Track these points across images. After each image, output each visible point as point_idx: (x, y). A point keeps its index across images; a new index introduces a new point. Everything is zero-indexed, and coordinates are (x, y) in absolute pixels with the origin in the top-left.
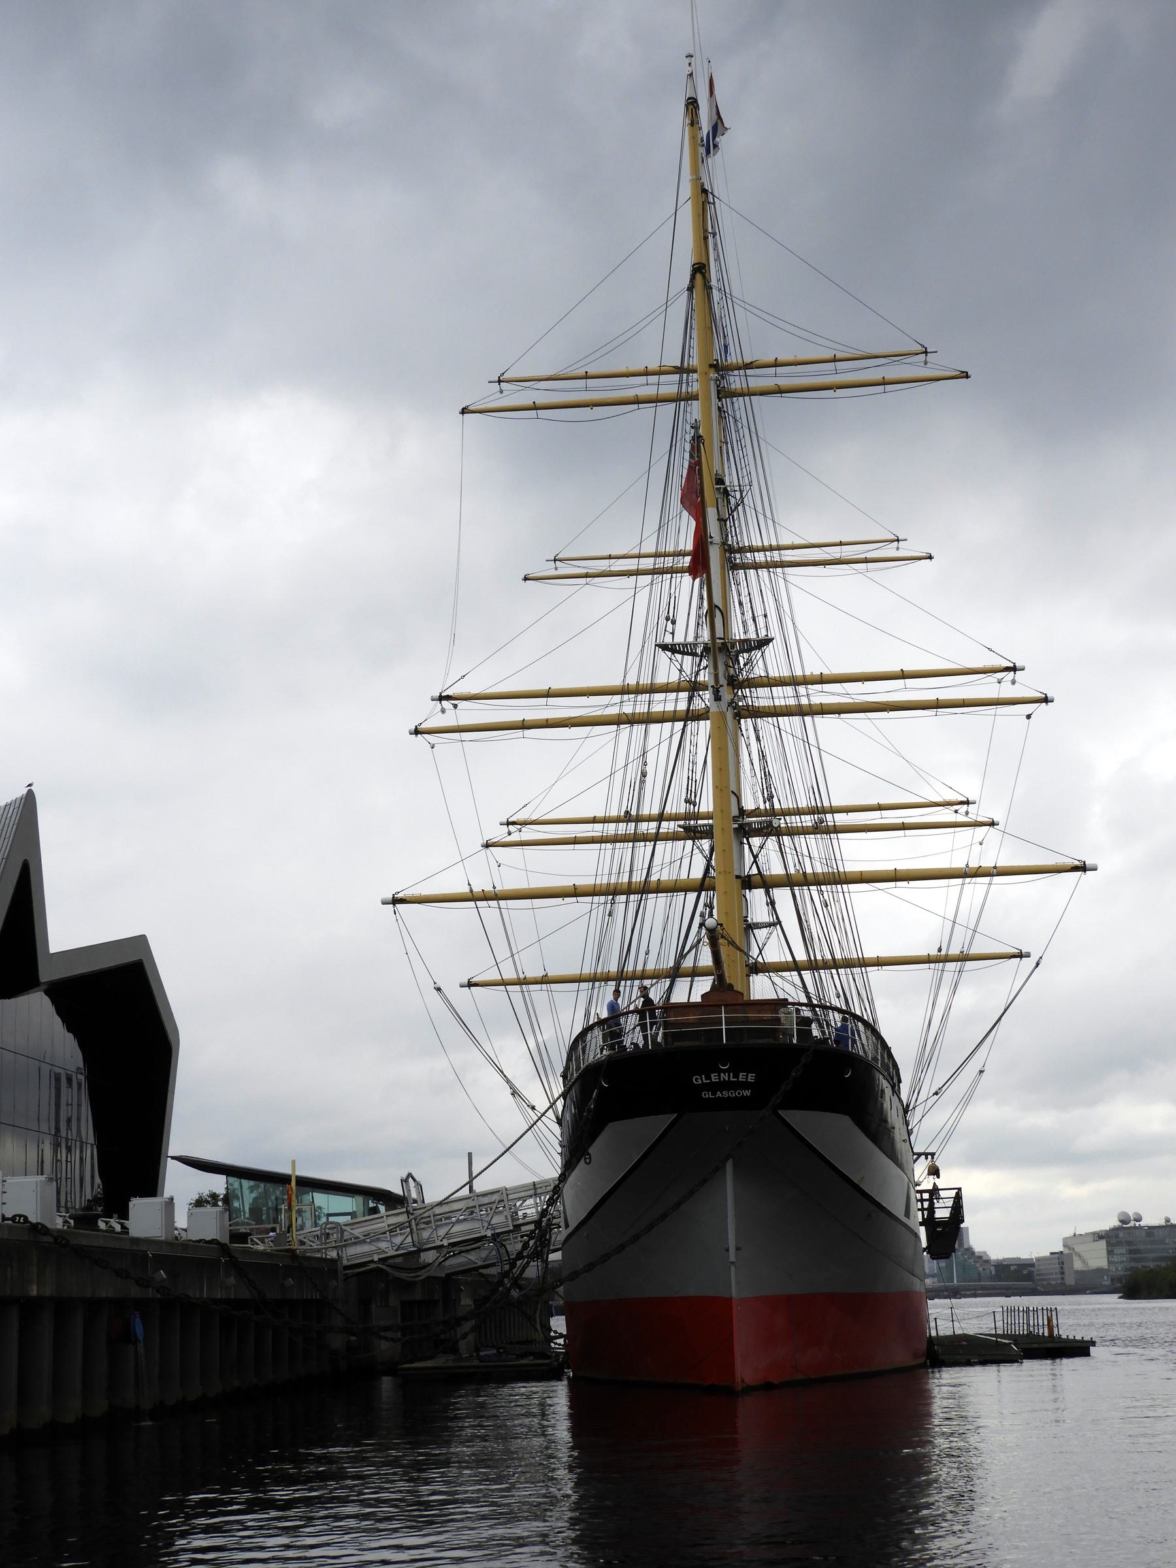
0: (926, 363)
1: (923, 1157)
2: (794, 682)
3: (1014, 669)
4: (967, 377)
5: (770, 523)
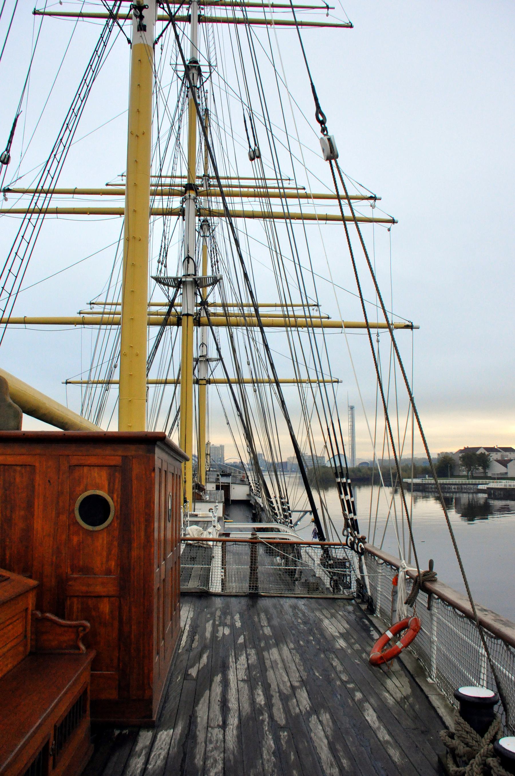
0: (327, 15)
1: (309, 513)
2: (239, 178)
3: (374, 198)
4: (351, 27)
5: (229, 139)
